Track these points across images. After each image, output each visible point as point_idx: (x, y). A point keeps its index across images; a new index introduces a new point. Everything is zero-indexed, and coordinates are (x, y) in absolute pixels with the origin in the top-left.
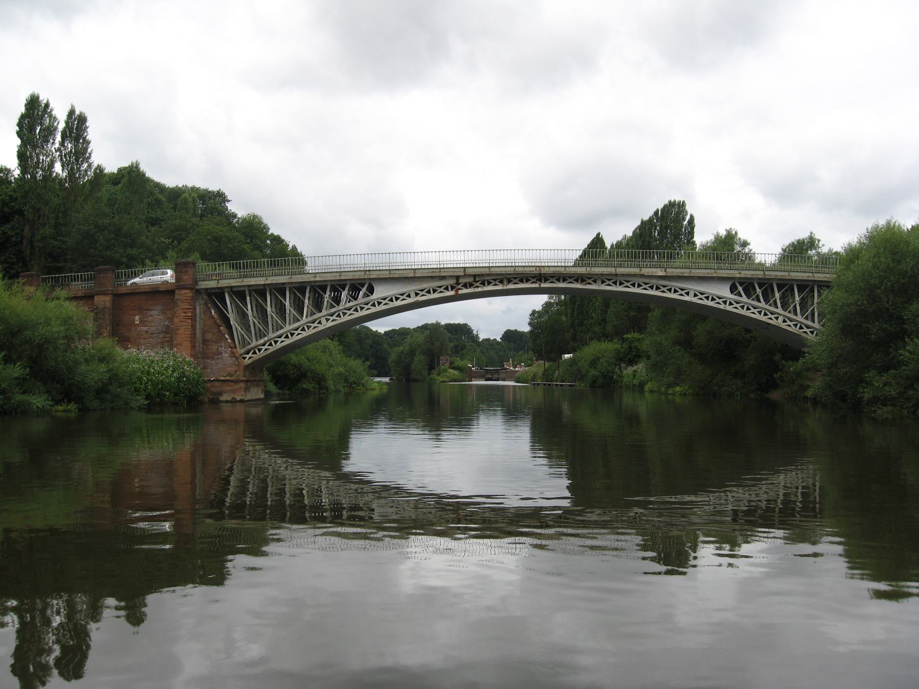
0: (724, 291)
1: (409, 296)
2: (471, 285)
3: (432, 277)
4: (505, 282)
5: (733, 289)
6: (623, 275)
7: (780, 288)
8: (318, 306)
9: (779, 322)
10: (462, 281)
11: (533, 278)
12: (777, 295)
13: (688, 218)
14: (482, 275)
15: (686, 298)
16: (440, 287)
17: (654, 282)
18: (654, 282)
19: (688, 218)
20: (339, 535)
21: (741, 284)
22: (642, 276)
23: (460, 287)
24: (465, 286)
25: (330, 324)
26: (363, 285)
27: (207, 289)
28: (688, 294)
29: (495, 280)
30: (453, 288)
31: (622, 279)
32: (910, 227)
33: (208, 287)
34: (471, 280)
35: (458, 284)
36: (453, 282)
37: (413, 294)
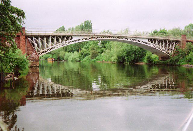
0: (146, 41)
1: (81, 40)
2: (95, 38)
4: (103, 37)
5: (148, 40)
7: (154, 40)
8: (58, 41)
9: (157, 48)
15: (139, 42)
18: (133, 39)
20: (50, 100)
21: (150, 40)
25: (157, 49)
26: (70, 37)
27: (28, 36)
28: (81, 40)
30: (91, 38)
31: (129, 38)
33: (29, 35)
34: (95, 37)
35: (92, 37)
36: (91, 37)
37: (82, 40)
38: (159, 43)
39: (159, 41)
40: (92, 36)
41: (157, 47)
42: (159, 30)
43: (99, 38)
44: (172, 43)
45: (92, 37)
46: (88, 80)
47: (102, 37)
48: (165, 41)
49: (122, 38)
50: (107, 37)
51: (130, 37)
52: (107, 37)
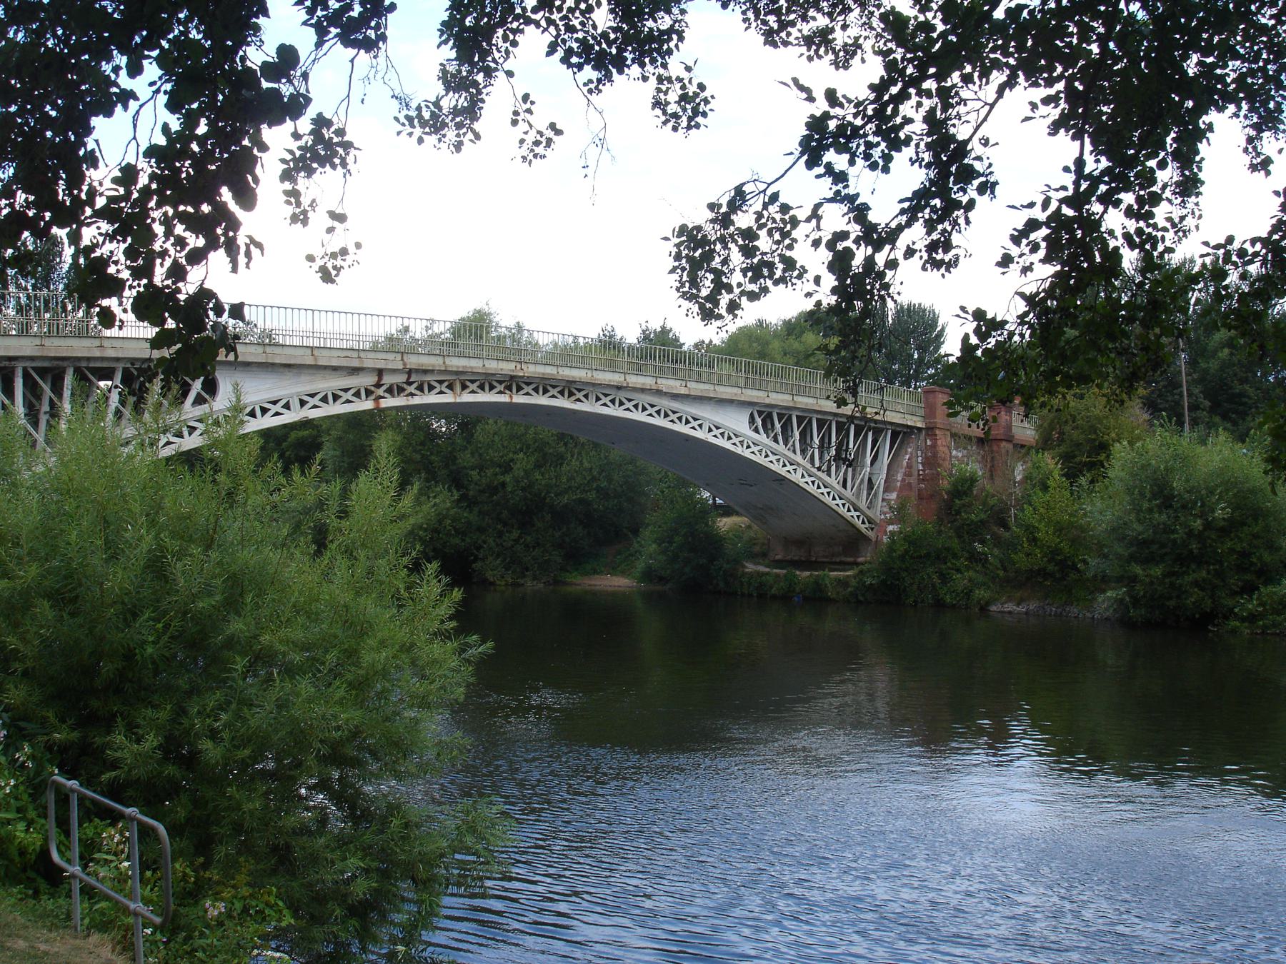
0: (738, 422)
1: (287, 406)
2: (401, 390)
3: (335, 369)
4: (458, 387)
5: (752, 420)
6: (635, 389)
10: (388, 380)
11: (500, 382)
12: (778, 426)
13: (665, 22)
14: (425, 372)
16: (346, 390)
17: (666, 403)
19: (665, 22)
22: (659, 393)
23: (381, 392)
24: (390, 391)
28: (287, 406)
29: (441, 382)
30: (369, 393)
32: (1066, 148)
34: (401, 379)
35: (378, 385)
36: (370, 380)
37: (295, 404)
38: (786, 428)
39: (770, 415)
40: (380, 372)
41: (800, 471)
42: (630, 335)
43: (431, 388)
44: (856, 436)
45: (378, 385)
46: (1010, 83)
47: (450, 387)
48: (821, 424)
49: (592, 397)
50: (487, 382)
51: (643, 390)
52: (492, 388)
